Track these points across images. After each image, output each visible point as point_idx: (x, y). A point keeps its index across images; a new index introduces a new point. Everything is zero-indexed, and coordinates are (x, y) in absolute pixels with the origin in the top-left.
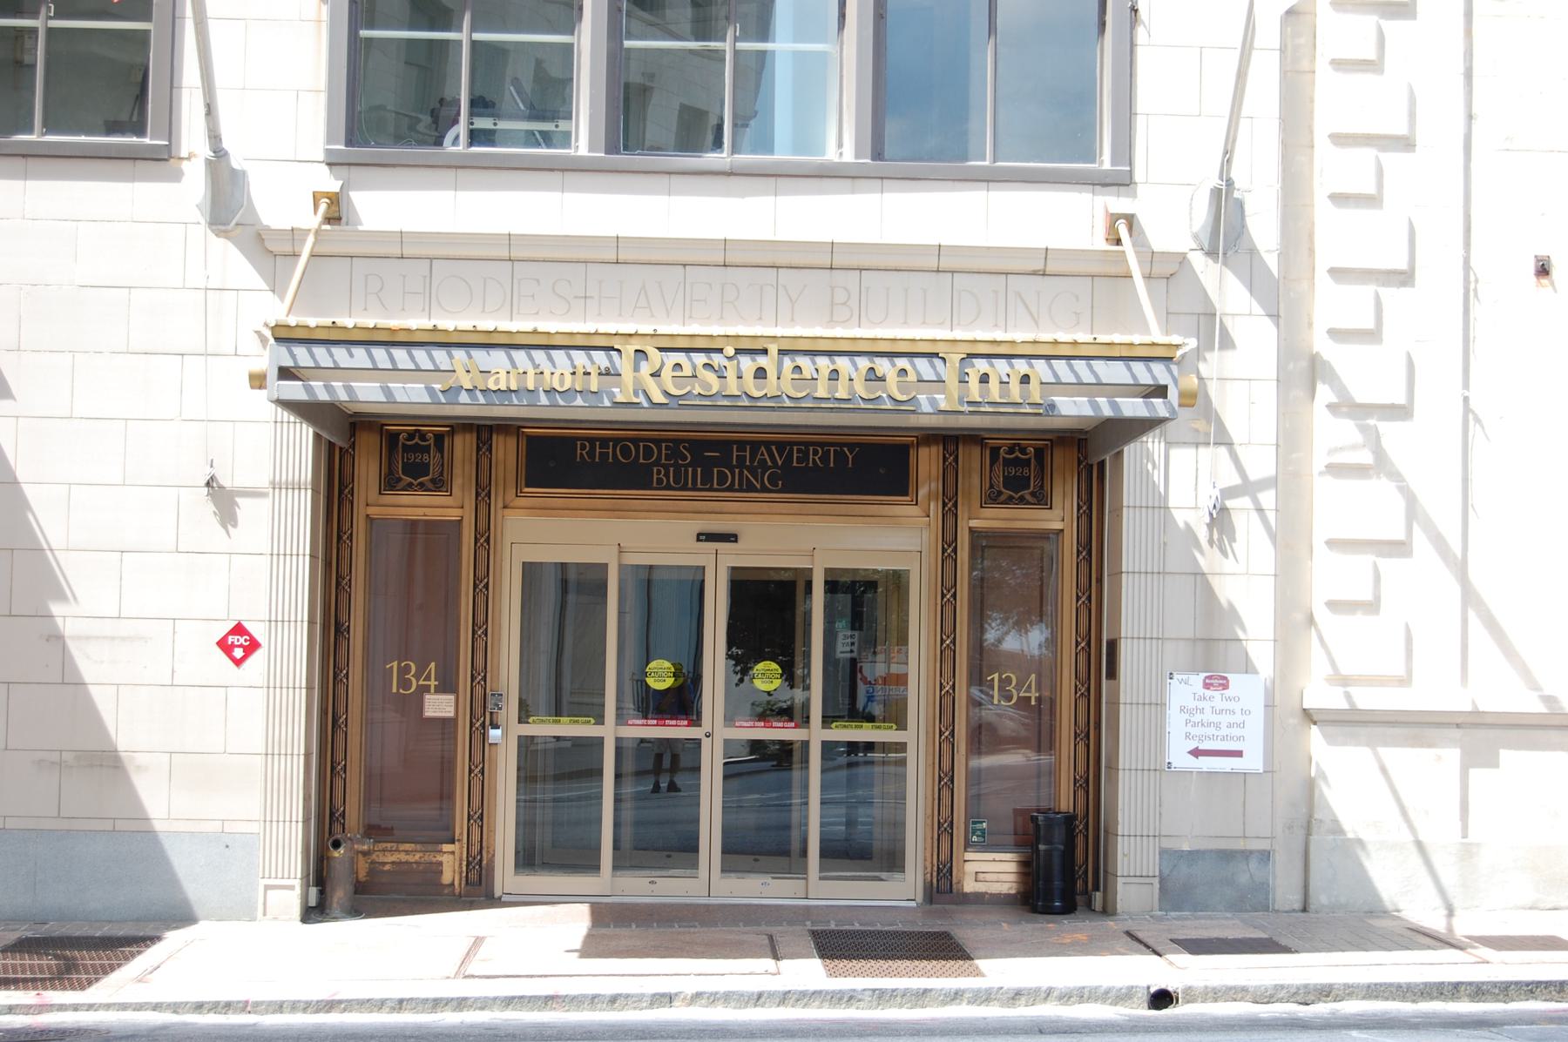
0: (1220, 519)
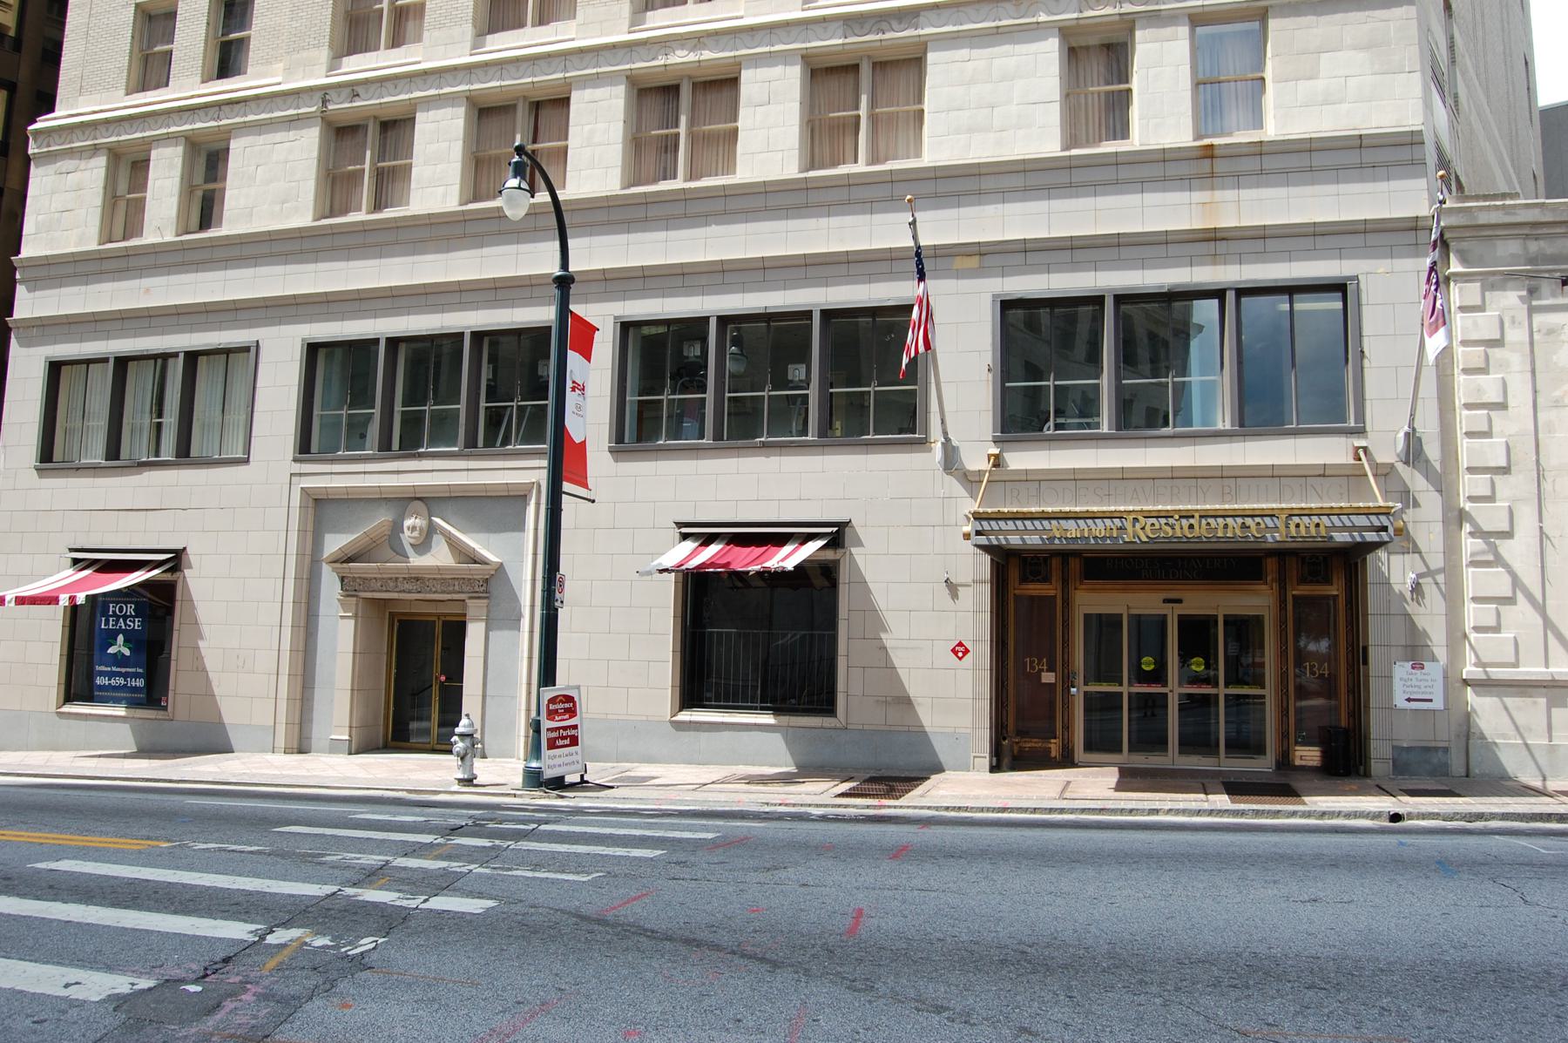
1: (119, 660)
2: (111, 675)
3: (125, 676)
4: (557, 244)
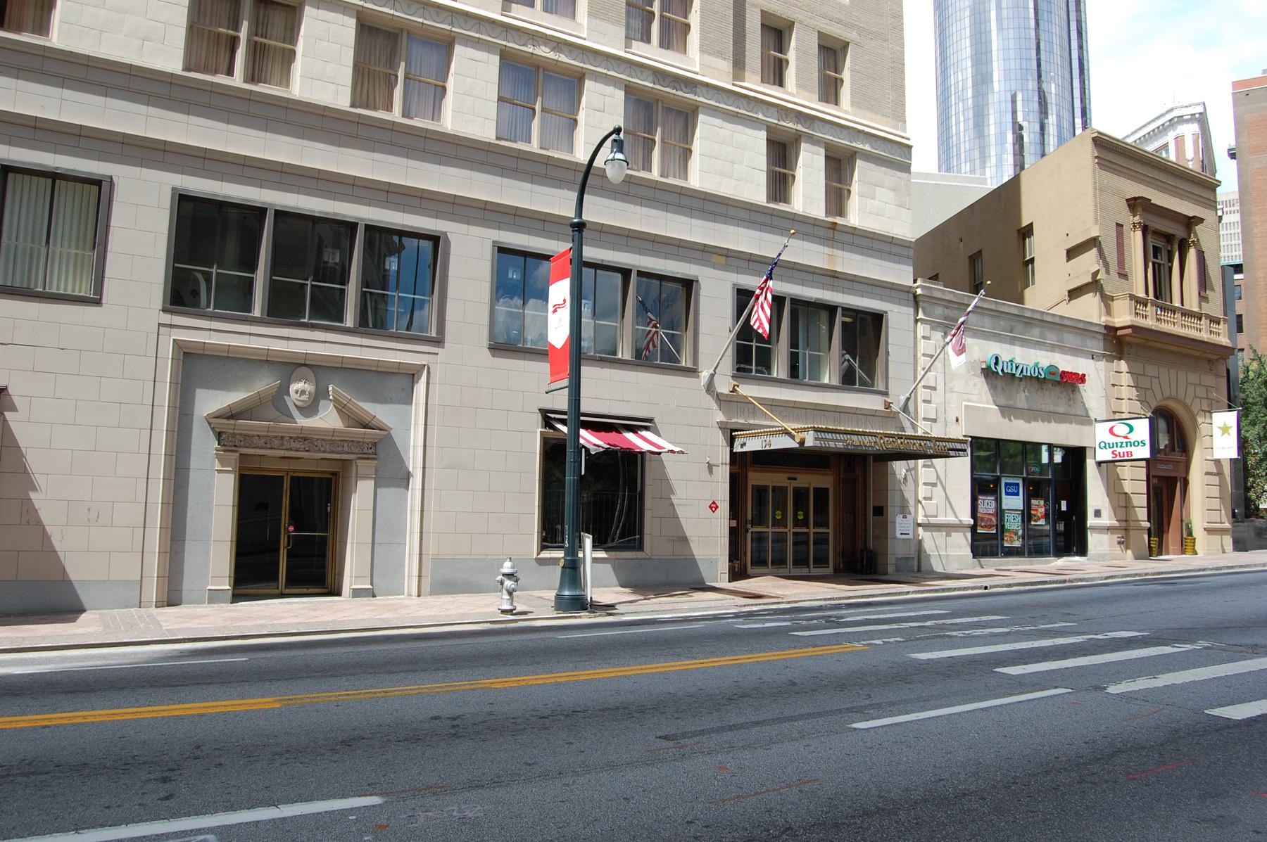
0: (905, 478)
4: (575, 195)
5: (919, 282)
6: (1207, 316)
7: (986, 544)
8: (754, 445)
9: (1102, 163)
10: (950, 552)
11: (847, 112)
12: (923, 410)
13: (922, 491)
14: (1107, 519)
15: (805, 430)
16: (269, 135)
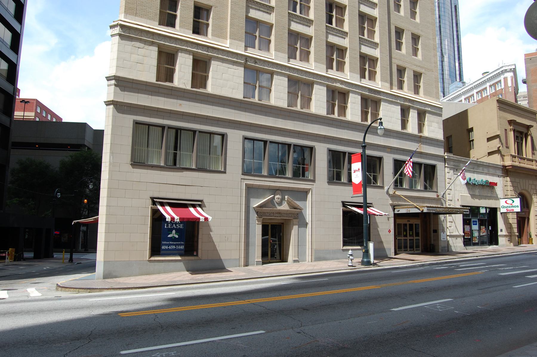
1: (173, 239)
2: (169, 245)
3: (175, 245)
5: (446, 154)
6: (535, 160)
7: (468, 242)
8: (403, 211)
9: (500, 108)
10: (457, 245)
11: (422, 97)
12: (448, 197)
13: (448, 224)
14: (504, 233)
15: (424, 207)
16: (267, 117)
